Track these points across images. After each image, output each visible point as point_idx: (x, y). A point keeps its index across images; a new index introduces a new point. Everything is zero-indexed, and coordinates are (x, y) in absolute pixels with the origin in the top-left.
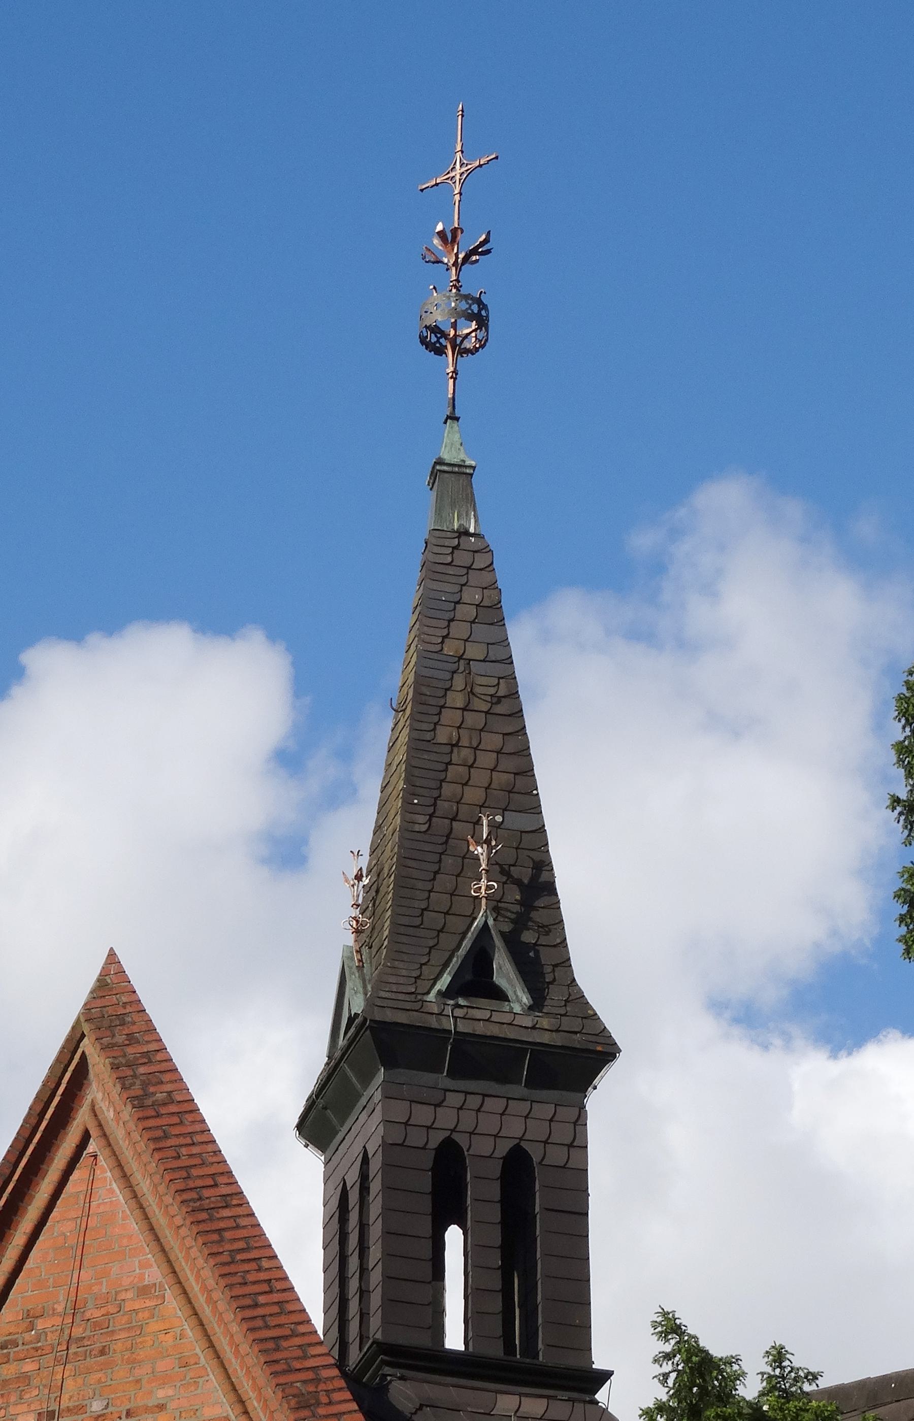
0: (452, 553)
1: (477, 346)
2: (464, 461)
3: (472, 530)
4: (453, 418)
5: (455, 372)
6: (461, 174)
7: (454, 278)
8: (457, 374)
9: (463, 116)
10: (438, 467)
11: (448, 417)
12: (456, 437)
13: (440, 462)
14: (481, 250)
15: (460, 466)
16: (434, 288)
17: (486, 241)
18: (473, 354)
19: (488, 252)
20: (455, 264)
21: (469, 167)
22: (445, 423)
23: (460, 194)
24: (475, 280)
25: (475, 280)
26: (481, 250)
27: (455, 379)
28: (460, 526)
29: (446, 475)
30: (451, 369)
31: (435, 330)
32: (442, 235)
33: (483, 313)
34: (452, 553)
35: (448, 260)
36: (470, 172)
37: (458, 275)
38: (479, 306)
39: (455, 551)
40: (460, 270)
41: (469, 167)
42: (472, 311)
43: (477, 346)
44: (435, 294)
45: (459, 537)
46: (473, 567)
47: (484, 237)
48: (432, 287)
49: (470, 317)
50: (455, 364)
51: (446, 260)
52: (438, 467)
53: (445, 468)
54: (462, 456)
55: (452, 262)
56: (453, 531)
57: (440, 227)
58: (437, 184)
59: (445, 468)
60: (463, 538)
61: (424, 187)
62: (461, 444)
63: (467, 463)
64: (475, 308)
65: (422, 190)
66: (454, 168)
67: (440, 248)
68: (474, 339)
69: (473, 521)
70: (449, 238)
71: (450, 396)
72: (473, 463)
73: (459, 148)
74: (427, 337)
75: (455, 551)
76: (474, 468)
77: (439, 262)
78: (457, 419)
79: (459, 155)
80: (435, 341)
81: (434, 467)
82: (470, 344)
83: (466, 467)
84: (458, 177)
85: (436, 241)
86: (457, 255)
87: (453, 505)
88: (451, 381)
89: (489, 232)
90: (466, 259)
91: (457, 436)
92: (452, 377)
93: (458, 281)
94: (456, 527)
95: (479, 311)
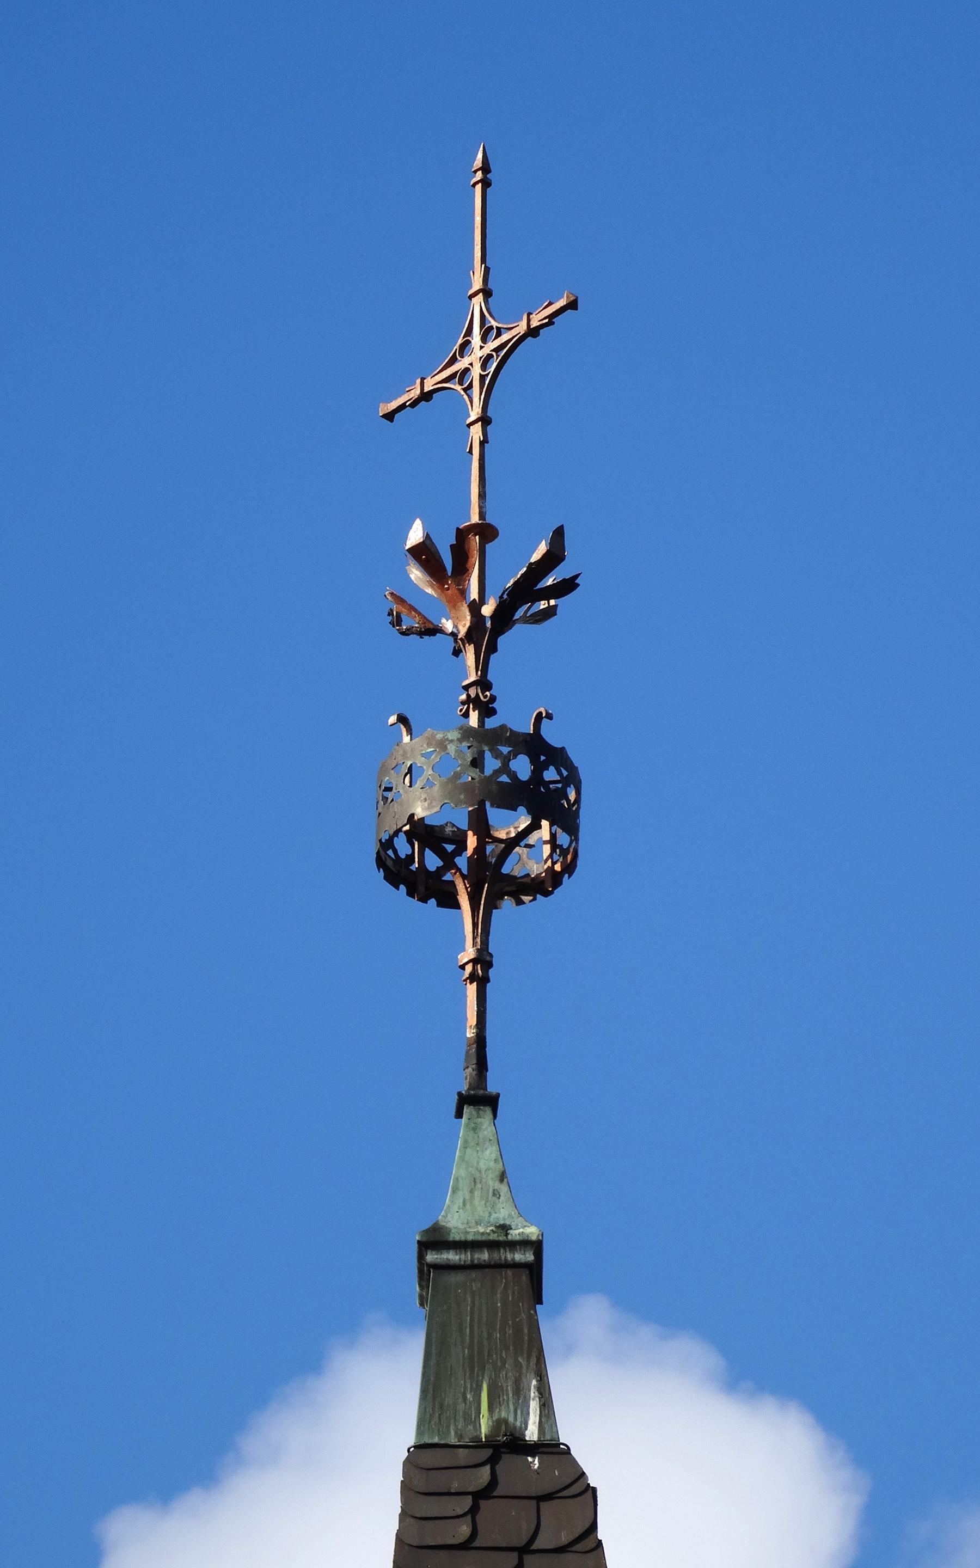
0: (474, 1511)
1: (558, 867)
2: (505, 1228)
3: (532, 1433)
4: (478, 1099)
5: (483, 960)
6: (486, 361)
7: (473, 678)
8: (487, 965)
9: (486, 183)
10: (431, 1257)
11: (464, 1101)
12: (488, 1157)
13: (435, 1239)
14: (532, 592)
15: (492, 1245)
16: (402, 719)
17: (553, 558)
18: (547, 894)
19: (567, 586)
20: (471, 636)
21: (505, 337)
22: (459, 1115)
23: (485, 420)
24: (535, 676)
25: (535, 676)
26: (532, 592)
27: (482, 982)
28: (498, 1425)
29: (455, 1279)
30: (470, 952)
31: (422, 832)
32: (424, 554)
33: (550, 774)
34: (474, 1511)
35: (456, 623)
36: (508, 351)
37: (483, 666)
38: (534, 760)
39: (483, 1503)
40: (492, 648)
41: (505, 337)
42: (513, 776)
43: (558, 867)
44: (406, 739)
45: (493, 1461)
46: (542, 1542)
47: (542, 548)
48: (393, 719)
49: (513, 795)
50: (484, 931)
51: (448, 626)
52: (431, 1257)
53: (452, 1257)
54: (504, 1213)
55: (463, 631)
56: (477, 1444)
57: (415, 535)
58: (426, 396)
59: (452, 1257)
60: (508, 1462)
61: (394, 405)
62: (502, 1177)
63: (515, 1234)
64: (522, 767)
65: (390, 416)
66: (466, 344)
67: (429, 591)
68: (547, 849)
69: (534, 1406)
70: (445, 563)
71: (470, 1033)
72: (532, 1231)
73: (477, 284)
74: (410, 858)
75: (483, 1503)
76: (537, 1246)
77: (432, 631)
78: (492, 1102)
79: (479, 300)
80: (420, 866)
81: (421, 1257)
82: (532, 861)
83: (513, 1245)
84: (476, 371)
85: (416, 574)
86: (475, 608)
87: (476, 1365)
88: (472, 989)
89: (558, 535)
90: (503, 618)
91: (490, 1152)
92: (472, 978)
93: (483, 683)
94: (484, 1430)
95: (538, 769)
